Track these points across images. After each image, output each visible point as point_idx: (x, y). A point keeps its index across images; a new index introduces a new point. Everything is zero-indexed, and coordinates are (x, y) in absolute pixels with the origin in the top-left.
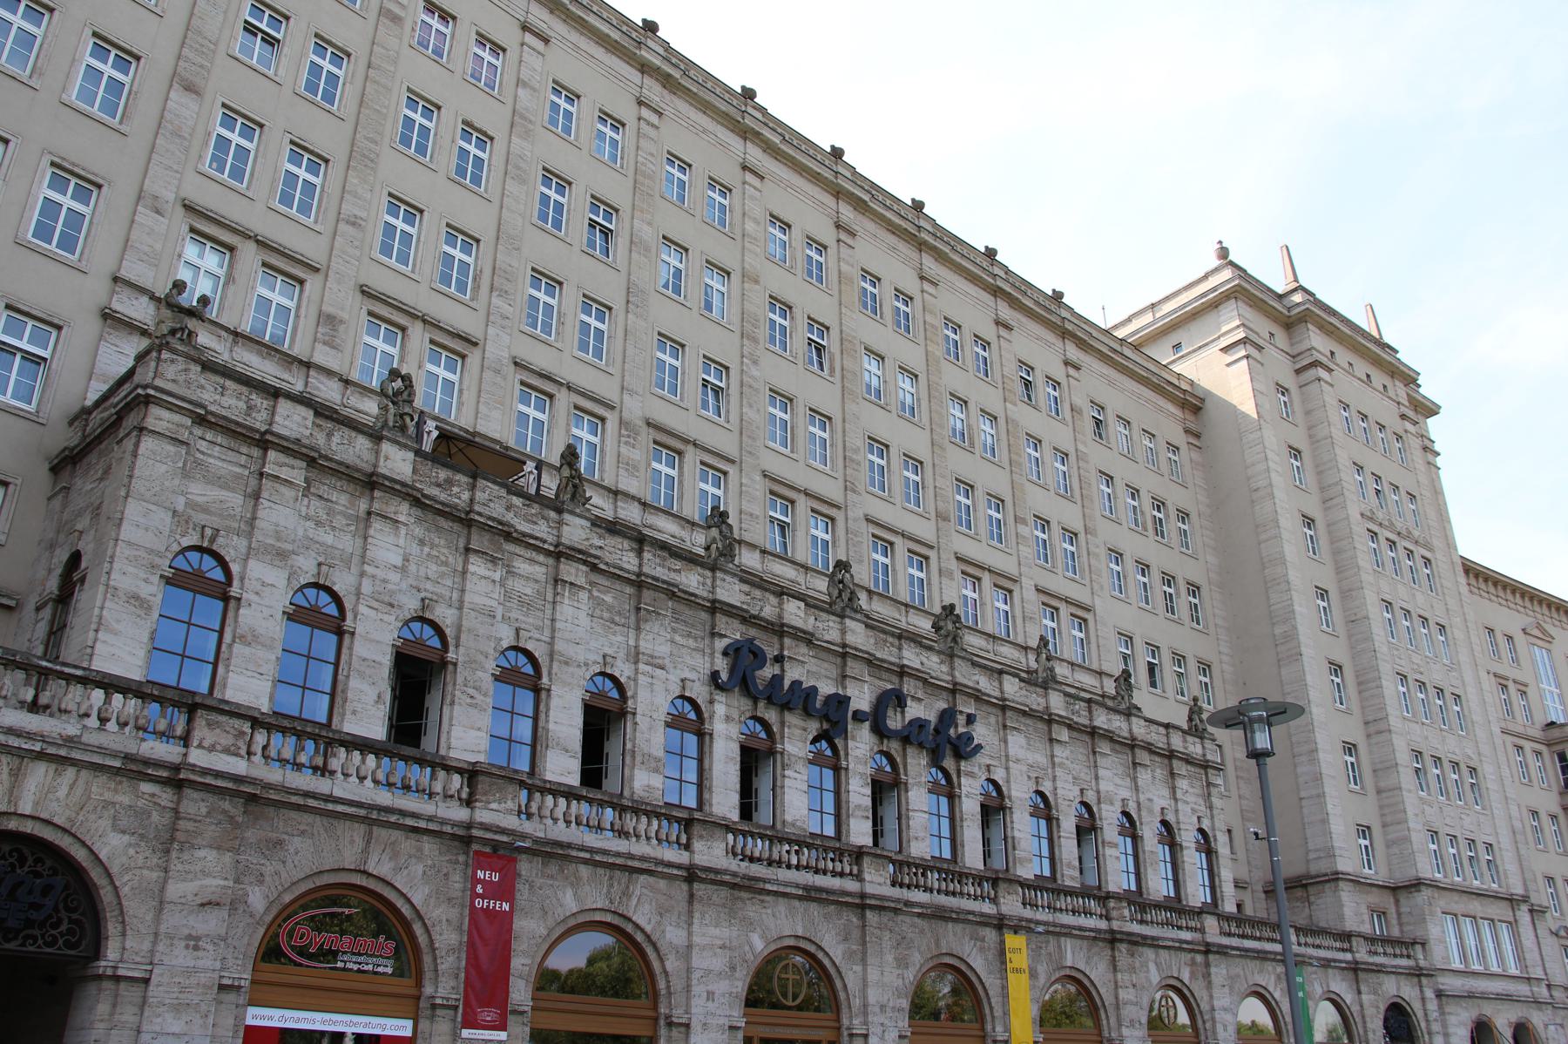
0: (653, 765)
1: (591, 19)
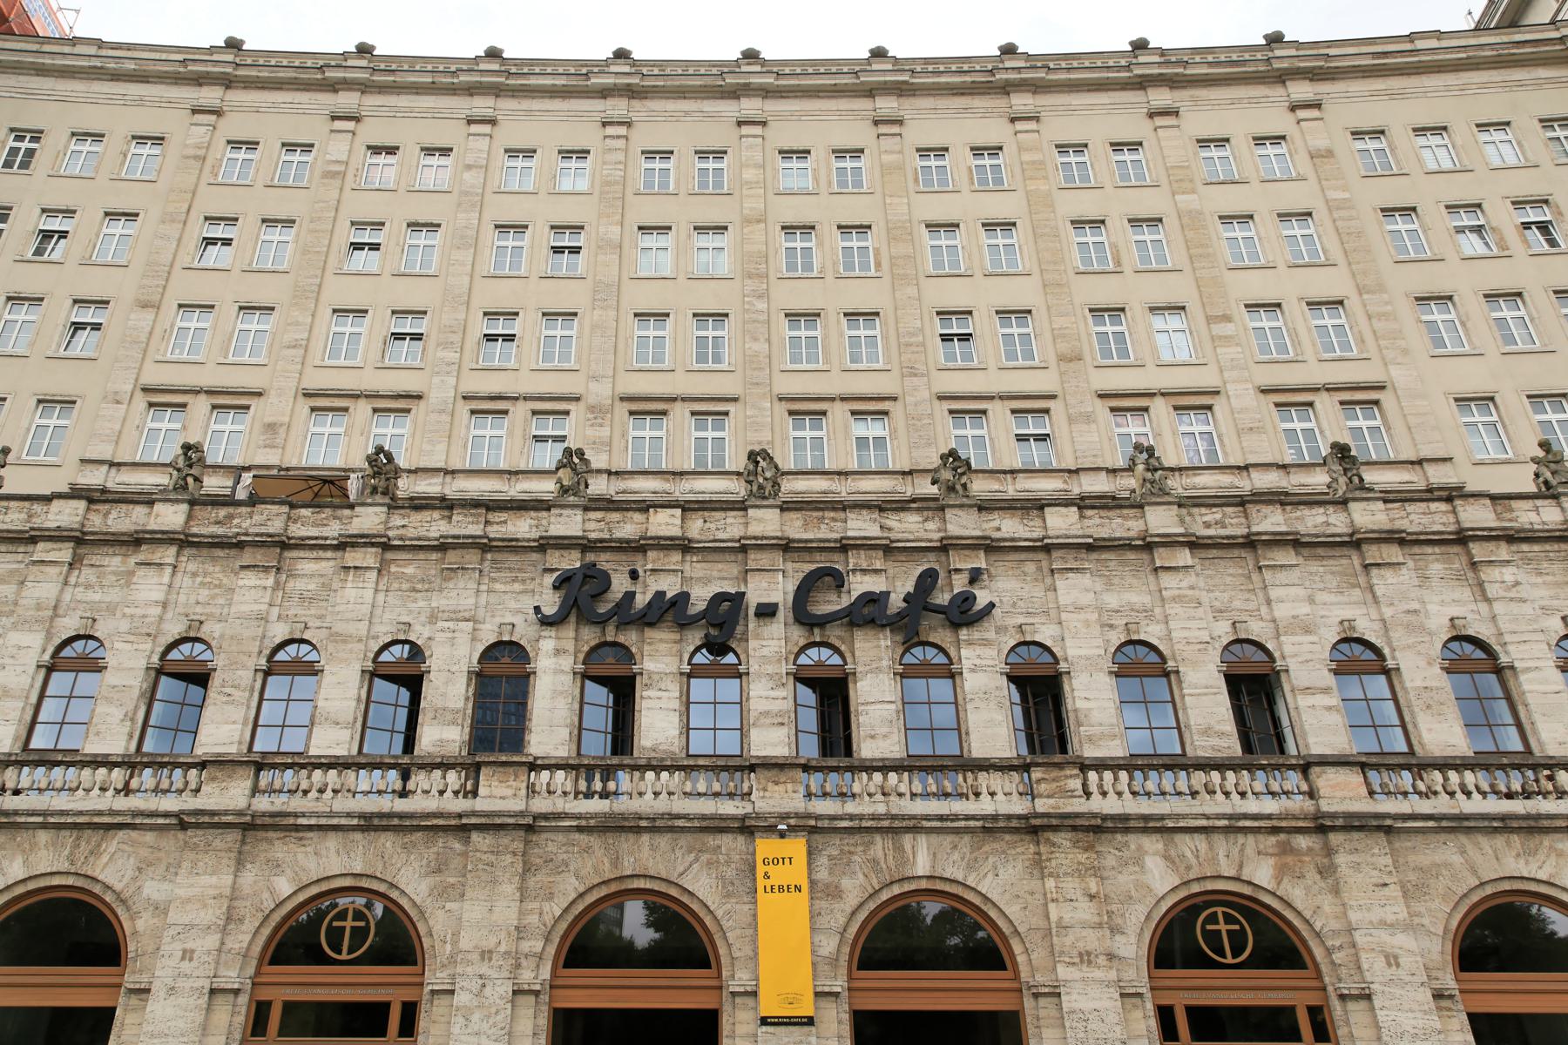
0: (449, 717)
1: (533, 81)
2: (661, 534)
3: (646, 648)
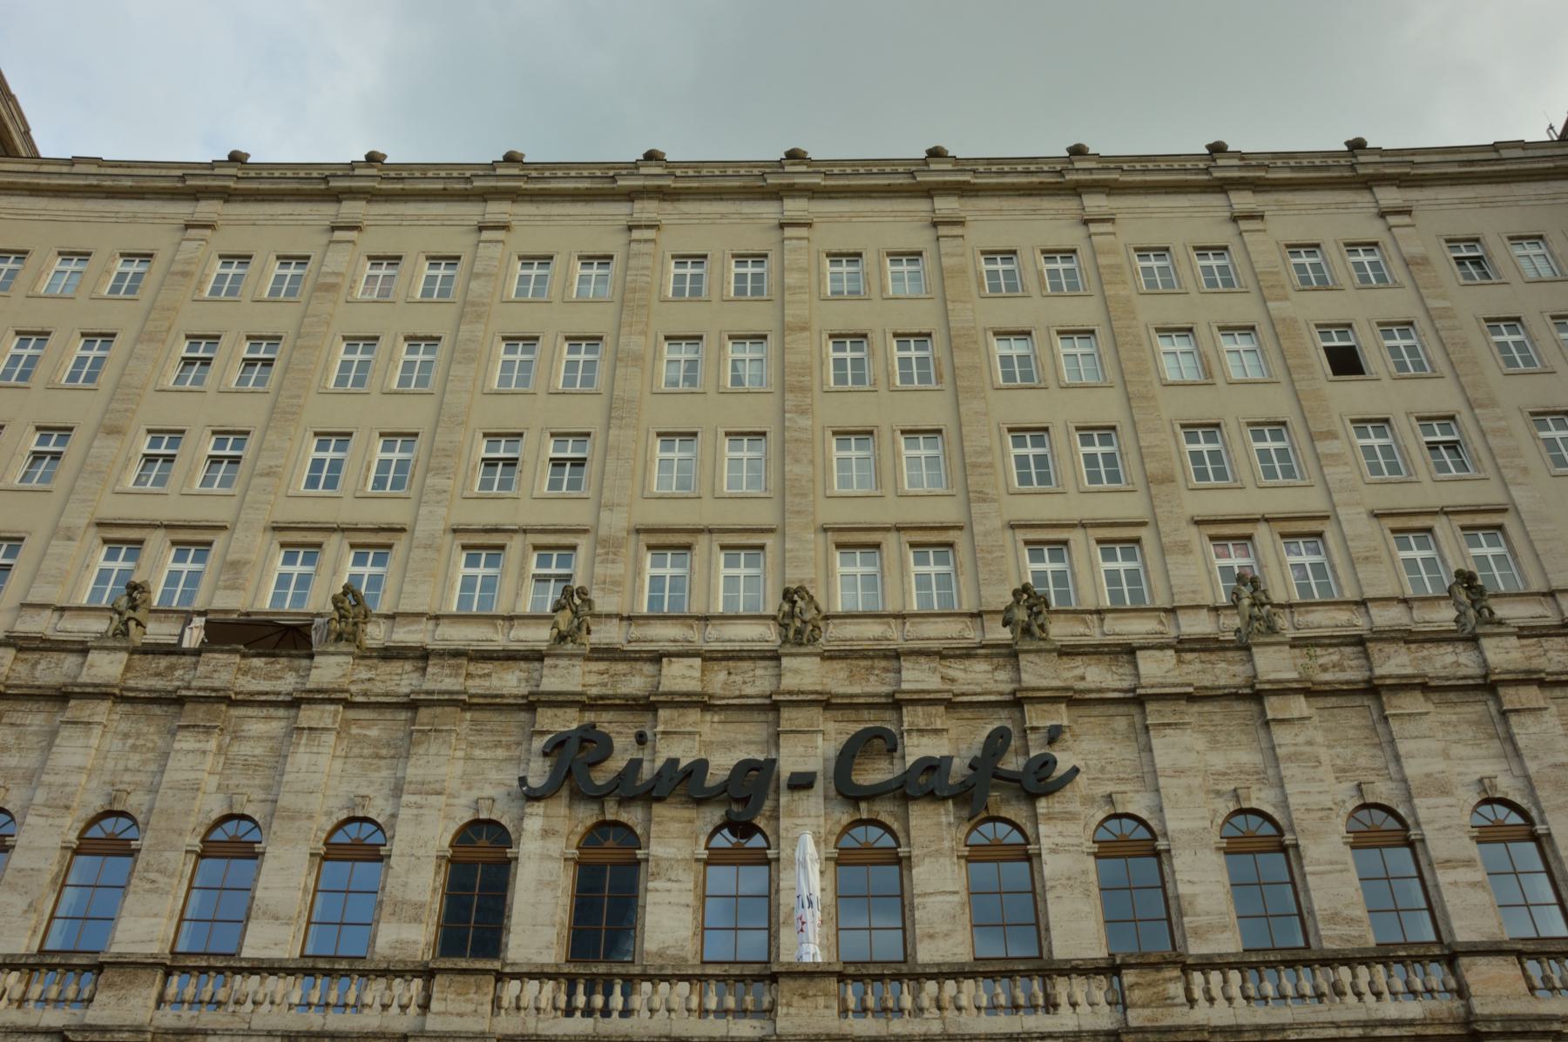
1: (554, 185)
2: (676, 688)
3: (654, 828)
